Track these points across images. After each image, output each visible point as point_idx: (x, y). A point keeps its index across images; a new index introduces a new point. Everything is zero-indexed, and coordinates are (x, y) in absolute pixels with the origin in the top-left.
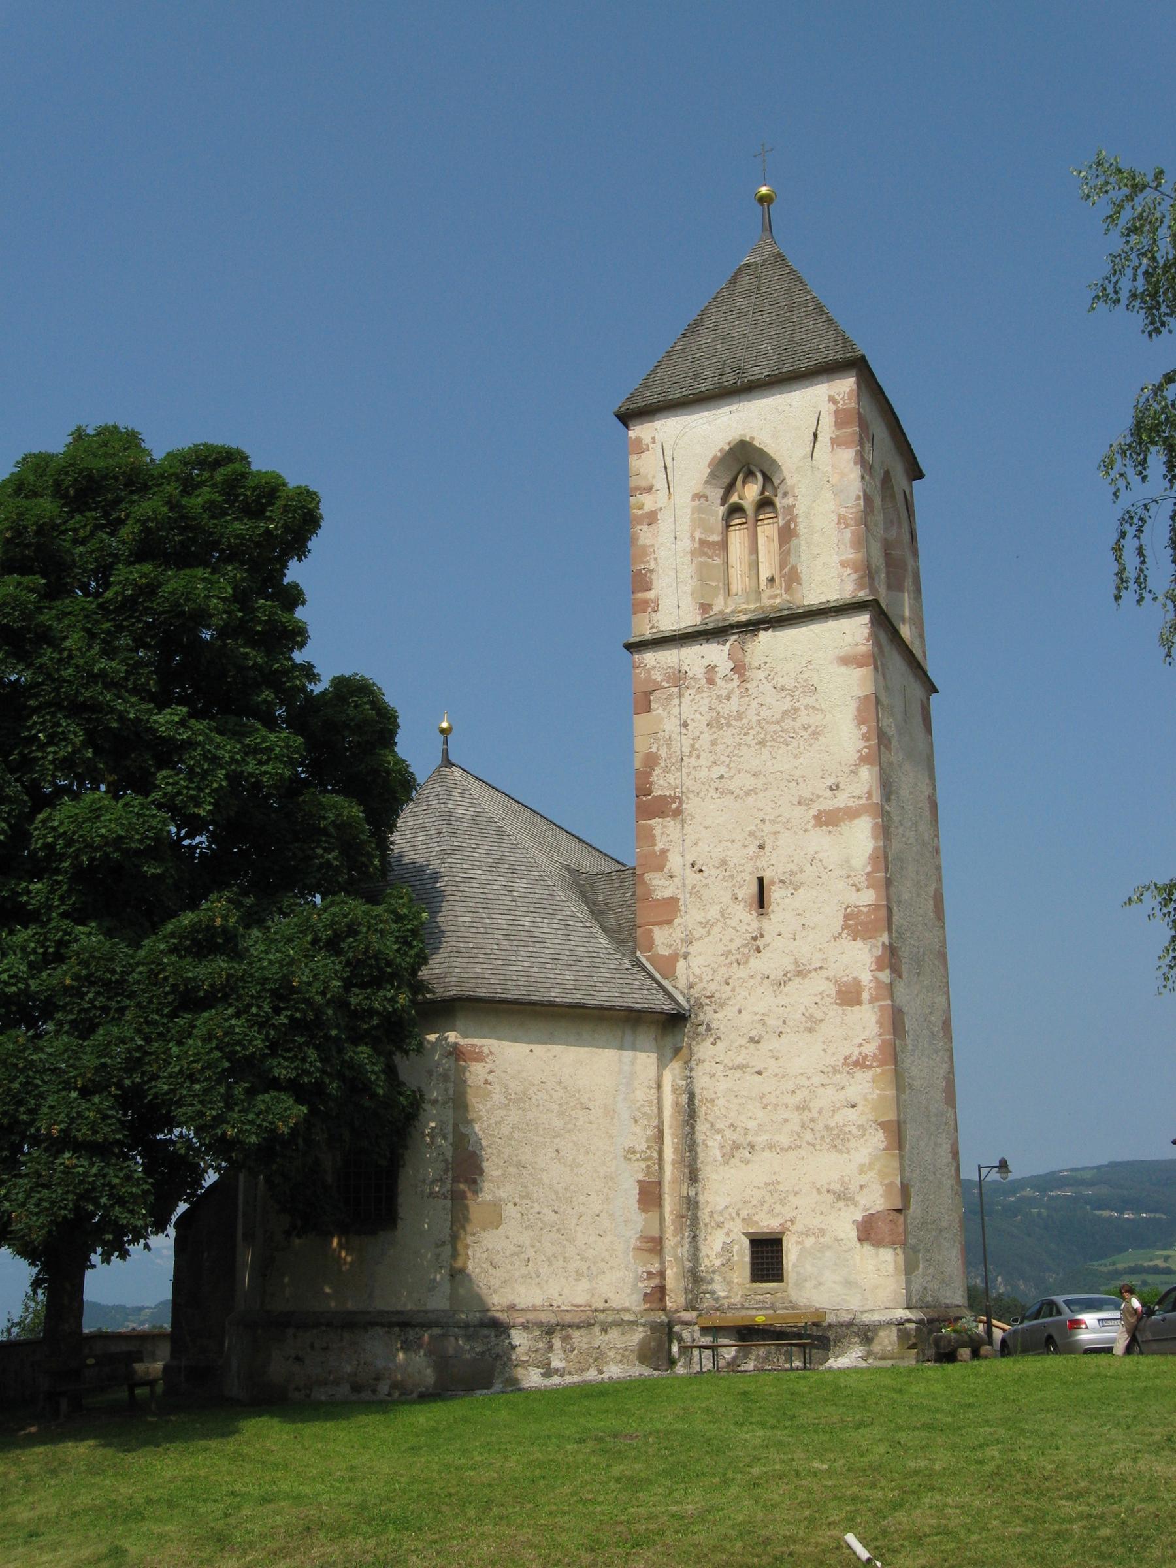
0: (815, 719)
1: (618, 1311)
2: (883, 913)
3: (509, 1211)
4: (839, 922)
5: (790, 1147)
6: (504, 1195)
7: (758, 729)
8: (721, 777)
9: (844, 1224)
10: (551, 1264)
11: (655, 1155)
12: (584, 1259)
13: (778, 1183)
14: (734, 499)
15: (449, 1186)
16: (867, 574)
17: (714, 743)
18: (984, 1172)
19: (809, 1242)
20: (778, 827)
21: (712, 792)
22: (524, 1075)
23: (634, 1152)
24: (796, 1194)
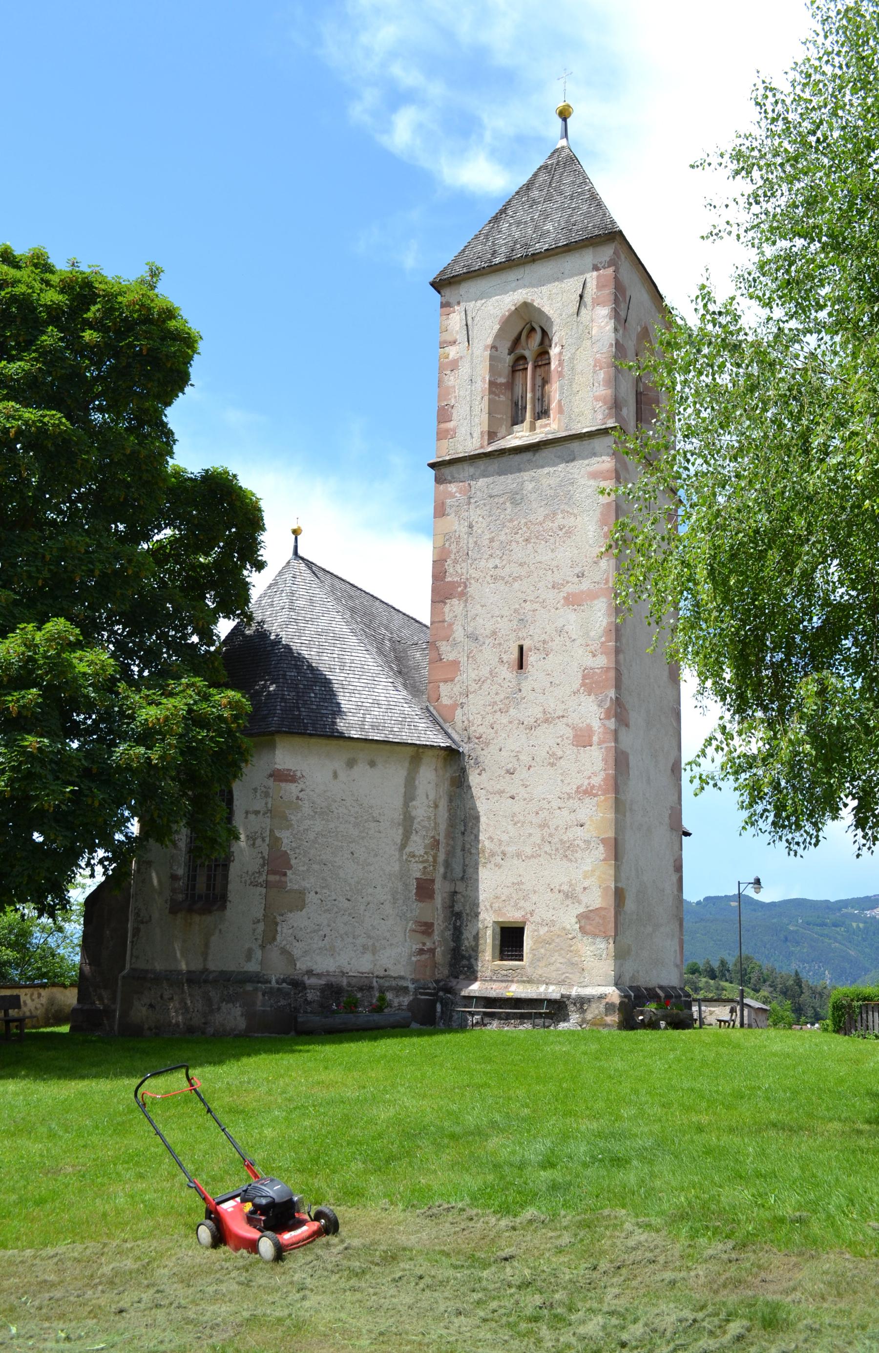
0: (570, 521)
1: (395, 978)
2: (612, 674)
3: (311, 897)
4: (577, 683)
5: (532, 856)
6: (308, 886)
7: (525, 529)
8: (496, 567)
9: (569, 919)
10: (343, 939)
11: (431, 859)
12: (369, 937)
13: (523, 883)
14: (519, 351)
15: (264, 877)
16: (616, 405)
17: (492, 540)
18: (742, 887)
19: (543, 930)
20: (536, 606)
21: (488, 578)
22: (329, 794)
23: (414, 856)
24: (535, 892)
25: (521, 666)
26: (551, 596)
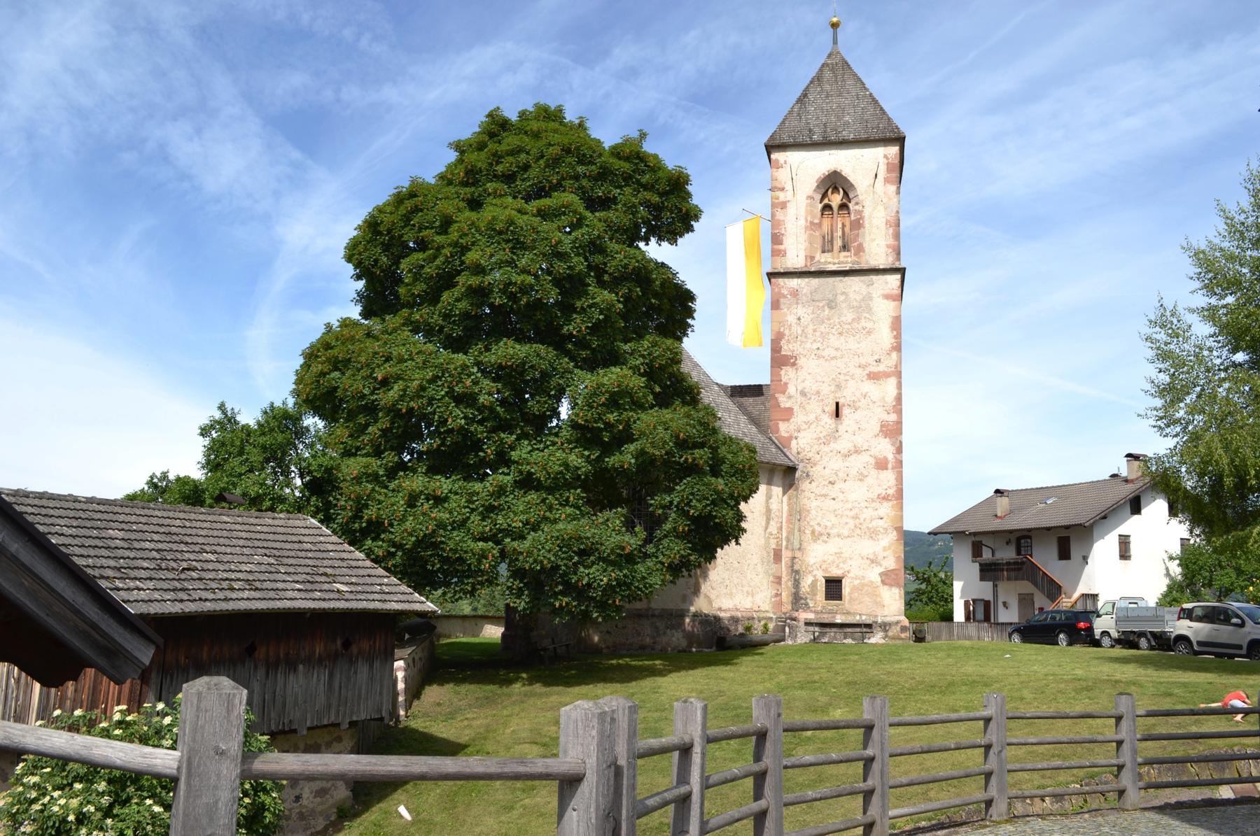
9: (874, 575)
25: (837, 415)
26: (859, 371)
